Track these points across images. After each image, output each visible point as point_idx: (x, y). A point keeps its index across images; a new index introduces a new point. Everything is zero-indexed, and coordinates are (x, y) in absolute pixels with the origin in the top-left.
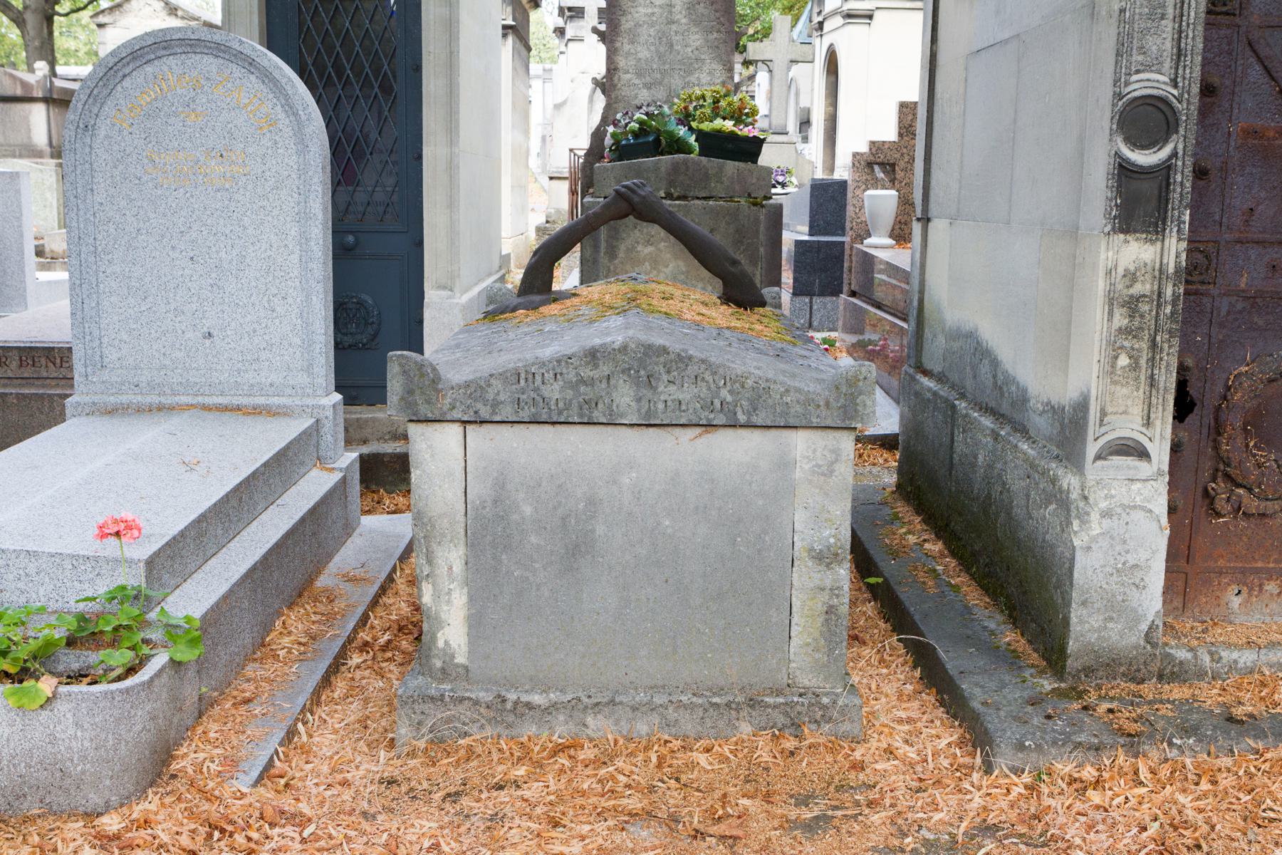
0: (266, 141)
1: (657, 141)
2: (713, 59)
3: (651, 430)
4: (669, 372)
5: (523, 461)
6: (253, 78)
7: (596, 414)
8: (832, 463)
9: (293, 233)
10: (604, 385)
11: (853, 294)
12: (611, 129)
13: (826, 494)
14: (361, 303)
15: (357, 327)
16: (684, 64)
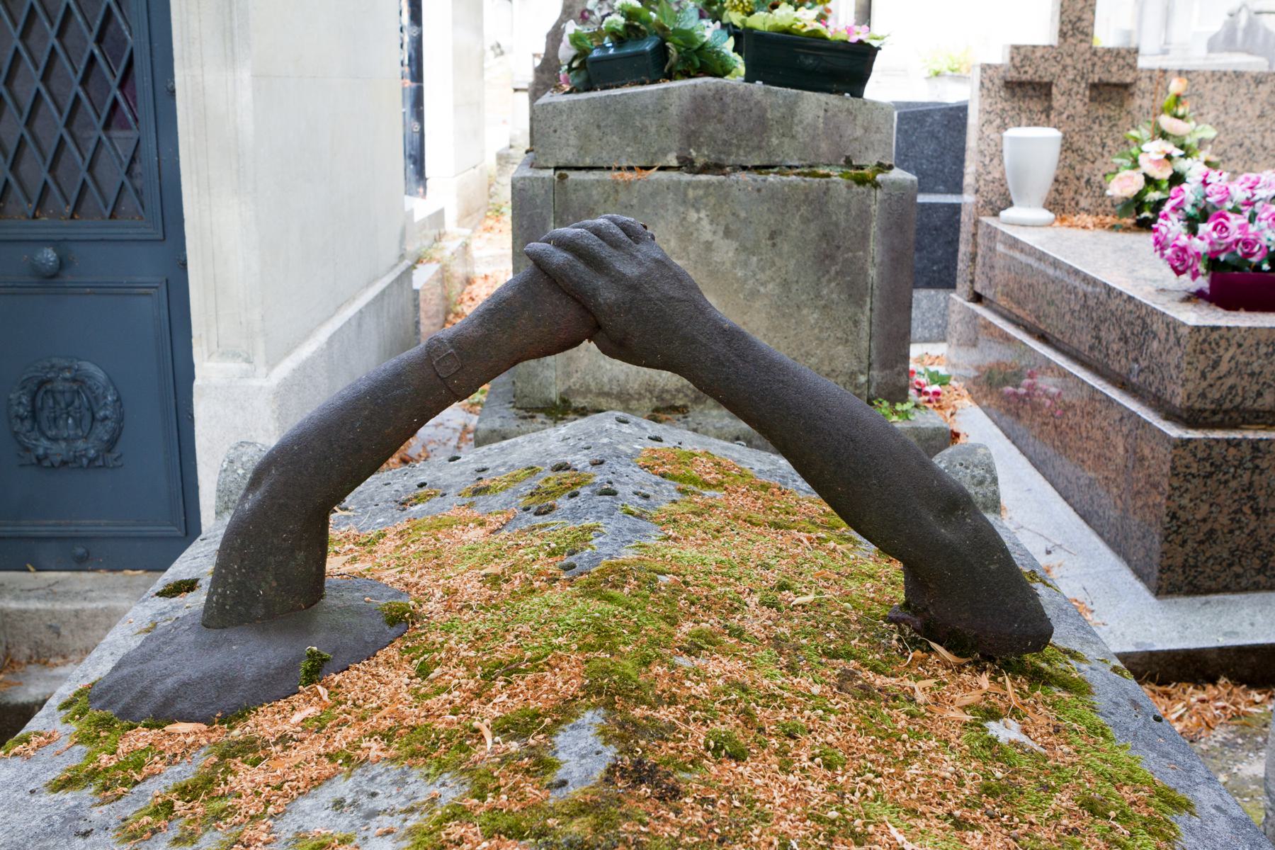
1: (661, 50)
11: (978, 298)
12: (571, 27)
14: (80, 381)
15: (78, 423)
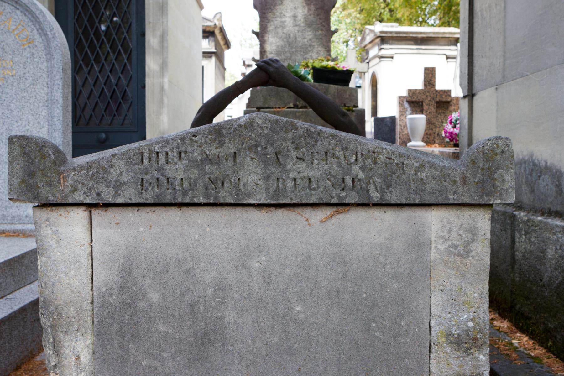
0: (27, 54)
2: (319, 45)
3: (280, 212)
4: (297, 148)
5: (149, 245)
6: (18, 12)
7: (222, 193)
8: (469, 243)
9: (44, 114)
10: (230, 163)
13: (463, 276)
16: (303, 48)
